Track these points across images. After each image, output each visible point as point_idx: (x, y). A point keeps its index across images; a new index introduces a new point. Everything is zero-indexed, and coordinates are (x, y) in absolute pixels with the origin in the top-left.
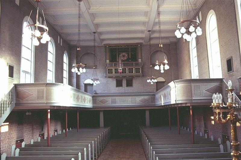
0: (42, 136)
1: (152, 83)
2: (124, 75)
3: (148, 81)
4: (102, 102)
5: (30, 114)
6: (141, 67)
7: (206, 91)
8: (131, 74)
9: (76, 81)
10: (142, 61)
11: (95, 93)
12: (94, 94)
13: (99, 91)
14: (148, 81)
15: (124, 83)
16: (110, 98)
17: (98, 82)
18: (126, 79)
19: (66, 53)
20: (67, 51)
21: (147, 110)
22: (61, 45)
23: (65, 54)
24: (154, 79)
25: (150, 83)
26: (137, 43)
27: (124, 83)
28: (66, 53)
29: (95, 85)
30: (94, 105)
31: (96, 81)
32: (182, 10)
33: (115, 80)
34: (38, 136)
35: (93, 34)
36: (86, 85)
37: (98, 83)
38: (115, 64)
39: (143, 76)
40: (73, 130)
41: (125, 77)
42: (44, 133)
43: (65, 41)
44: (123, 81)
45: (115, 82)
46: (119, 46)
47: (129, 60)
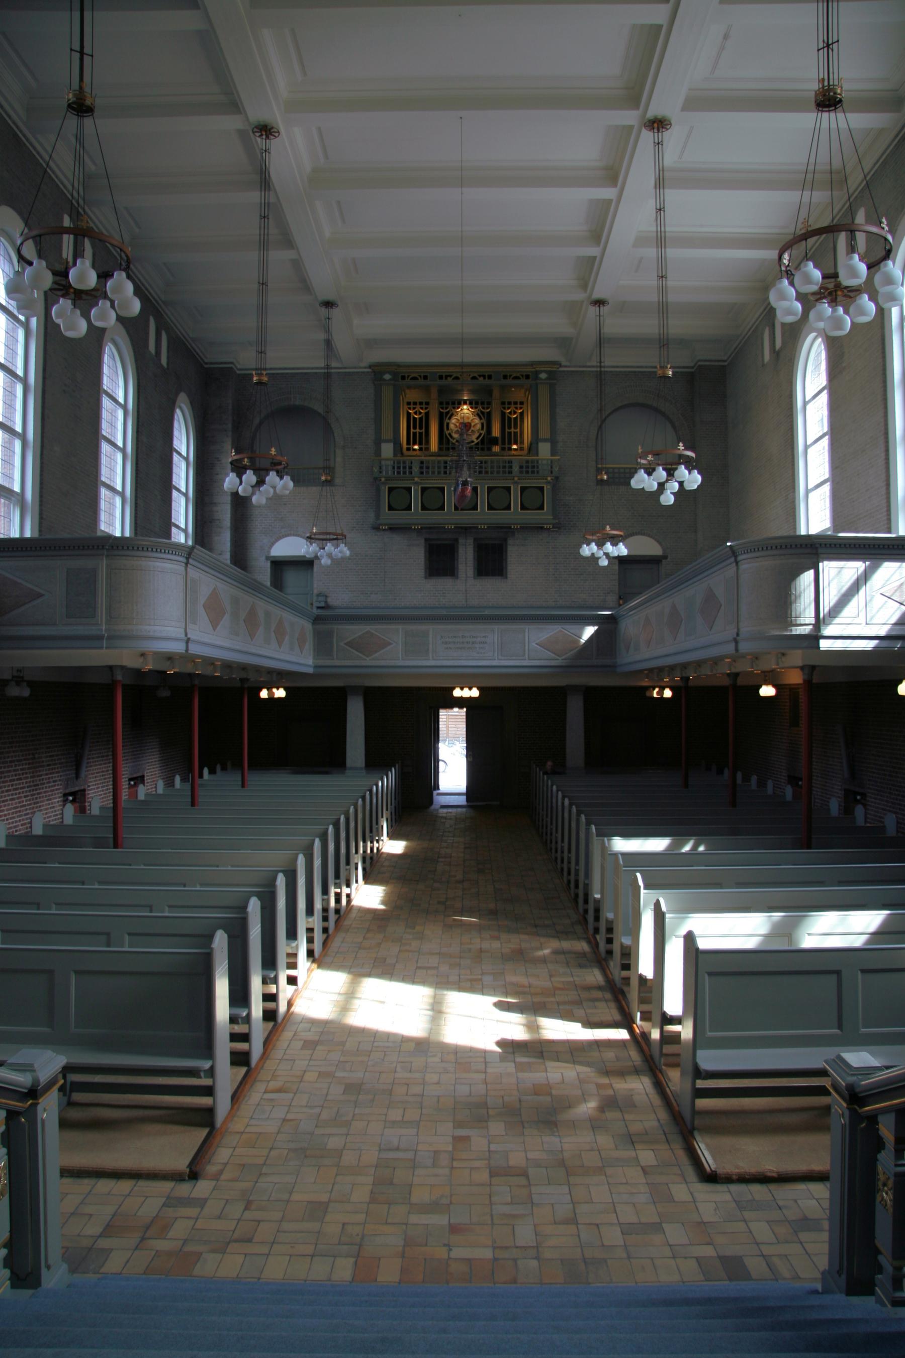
0: (78, 797)
1: (604, 562)
2: (466, 518)
3: (587, 550)
4: (360, 646)
5: (26, 692)
6: (548, 483)
7: (537, 644)
8: (500, 517)
9: (228, 544)
10: (553, 452)
11: (322, 604)
12: (318, 608)
13: (340, 598)
14: (587, 550)
15: (466, 555)
16: (400, 627)
17: (344, 550)
18: (475, 540)
19: (183, 405)
20: (189, 396)
21: (574, 689)
22: (164, 361)
23: (178, 411)
24: (615, 541)
25: (594, 559)
26: (532, 364)
27: (466, 555)
28: (183, 405)
29: (325, 561)
30: (321, 662)
31: (329, 547)
32: (811, 168)
33: (423, 541)
34: (57, 800)
35: (323, 309)
36: (279, 566)
37: (340, 555)
38: (422, 462)
39: (558, 527)
40: (213, 777)
41: (465, 530)
42: (84, 790)
43: (179, 346)
44: (461, 551)
45: (418, 554)
46: (447, 377)
47: (489, 449)
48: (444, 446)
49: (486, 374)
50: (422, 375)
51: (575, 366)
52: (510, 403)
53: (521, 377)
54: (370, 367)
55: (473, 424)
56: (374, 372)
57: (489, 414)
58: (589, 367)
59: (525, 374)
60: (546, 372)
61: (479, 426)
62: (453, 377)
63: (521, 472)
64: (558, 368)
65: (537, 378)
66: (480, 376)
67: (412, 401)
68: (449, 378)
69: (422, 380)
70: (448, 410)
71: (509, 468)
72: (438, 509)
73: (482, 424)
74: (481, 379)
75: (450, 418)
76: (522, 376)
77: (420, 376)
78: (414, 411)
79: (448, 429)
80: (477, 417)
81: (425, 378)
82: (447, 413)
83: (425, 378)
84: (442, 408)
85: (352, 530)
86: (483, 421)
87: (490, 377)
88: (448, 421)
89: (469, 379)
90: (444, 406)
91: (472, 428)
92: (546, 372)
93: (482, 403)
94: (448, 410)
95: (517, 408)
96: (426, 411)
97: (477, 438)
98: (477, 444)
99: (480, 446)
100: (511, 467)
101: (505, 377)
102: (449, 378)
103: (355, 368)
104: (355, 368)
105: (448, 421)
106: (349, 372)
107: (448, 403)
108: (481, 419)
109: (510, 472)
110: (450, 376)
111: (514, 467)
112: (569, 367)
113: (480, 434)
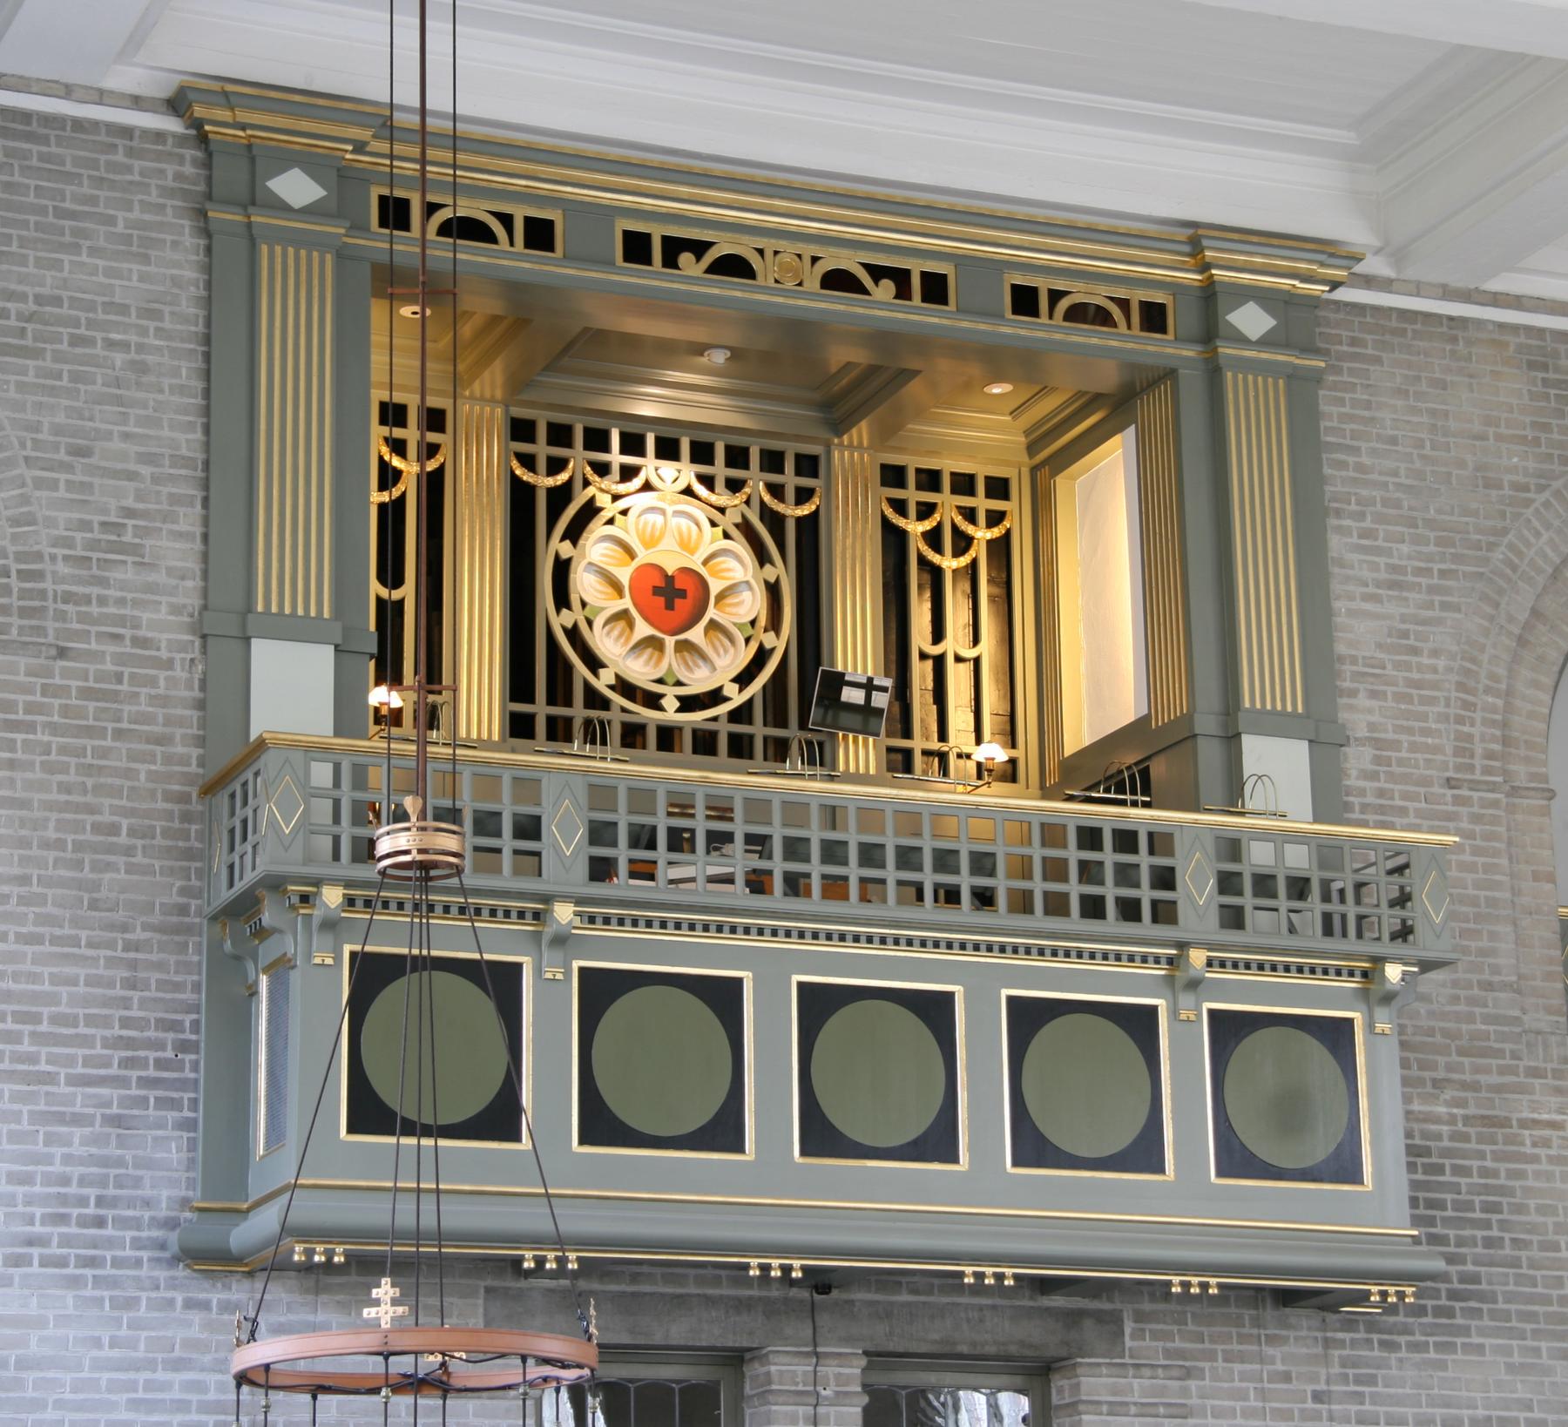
10: (1328, 801)
48: (541, 709)
49: (520, 213)
50: (520, 213)
51: (1418, 290)
52: (930, 480)
53: (497, 227)
54: (177, 104)
55: (715, 587)
56: (203, 139)
57: (809, 527)
58: (1497, 300)
59: (1138, 295)
60: (1266, 298)
61: (752, 604)
62: (710, 257)
63: (601, 870)
64: (1335, 285)
65: (1210, 331)
66: (877, 273)
67: (982, 470)
68: (686, 258)
69: (1136, 330)
70: (563, 477)
71: (634, 843)
72: (916, 1150)
73: (773, 590)
74: (885, 290)
75: (574, 533)
76: (1124, 304)
77: (506, 220)
78: (927, 525)
79: (562, 599)
80: (740, 547)
81: (540, 235)
82: (559, 497)
83: (540, 235)
84: (528, 462)
85: (18, 1261)
86: (782, 572)
87: (935, 288)
88: (566, 549)
89: (813, 283)
90: (542, 449)
91: (711, 613)
92: (1266, 298)
93: (772, 461)
94: (563, 477)
95: (970, 515)
96: (996, 532)
97: (743, 679)
98: (741, 714)
99: (758, 729)
100: (1165, 879)
101: (1025, 301)
102: (686, 258)
103: (68, 91)
104: (68, 91)
105: (566, 549)
106: (26, 116)
107: (559, 434)
108: (762, 557)
109: (1164, 913)
110: (699, 248)
111: (1184, 879)
112: (1385, 285)
113: (762, 656)
